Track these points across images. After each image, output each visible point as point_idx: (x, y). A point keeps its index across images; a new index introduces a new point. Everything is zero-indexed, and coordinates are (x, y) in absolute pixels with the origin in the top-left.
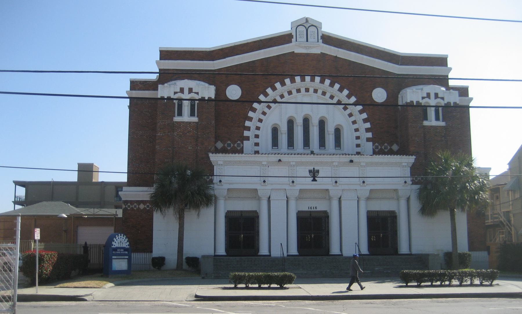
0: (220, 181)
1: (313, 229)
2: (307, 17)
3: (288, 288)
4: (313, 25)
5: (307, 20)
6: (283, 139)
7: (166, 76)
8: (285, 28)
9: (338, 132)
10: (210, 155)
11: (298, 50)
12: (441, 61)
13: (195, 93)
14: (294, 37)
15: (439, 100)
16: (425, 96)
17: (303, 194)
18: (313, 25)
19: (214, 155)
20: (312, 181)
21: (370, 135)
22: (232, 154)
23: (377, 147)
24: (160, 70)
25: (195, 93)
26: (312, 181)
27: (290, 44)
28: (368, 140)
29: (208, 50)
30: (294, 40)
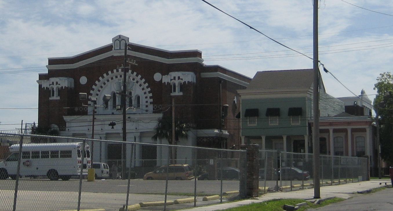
0: (68, 130)
1: (16, 159)
2: (120, 34)
3: (312, 197)
4: (123, 39)
5: (120, 36)
6: (110, 103)
7: (52, 74)
8: (109, 42)
9: (138, 98)
10: (64, 117)
11: (115, 55)
12: (197, 54)
13: (59, 84)
14: (114, 46)
15: (180, 80)
16: (173, 78)
17: (108, 135)
18: (123, 39)
19: (65, 117)
20: (112, 128)
21: (152, 100)
22: (73, 116)
23: (155, 107)
24: (49, 71)
25: (59, 84)
26: (112, 128)
27: (111, 51)
28: (151, 103)
29: (71, 58)
30: (113, 49)
